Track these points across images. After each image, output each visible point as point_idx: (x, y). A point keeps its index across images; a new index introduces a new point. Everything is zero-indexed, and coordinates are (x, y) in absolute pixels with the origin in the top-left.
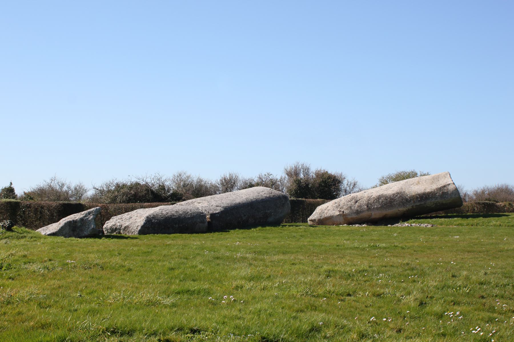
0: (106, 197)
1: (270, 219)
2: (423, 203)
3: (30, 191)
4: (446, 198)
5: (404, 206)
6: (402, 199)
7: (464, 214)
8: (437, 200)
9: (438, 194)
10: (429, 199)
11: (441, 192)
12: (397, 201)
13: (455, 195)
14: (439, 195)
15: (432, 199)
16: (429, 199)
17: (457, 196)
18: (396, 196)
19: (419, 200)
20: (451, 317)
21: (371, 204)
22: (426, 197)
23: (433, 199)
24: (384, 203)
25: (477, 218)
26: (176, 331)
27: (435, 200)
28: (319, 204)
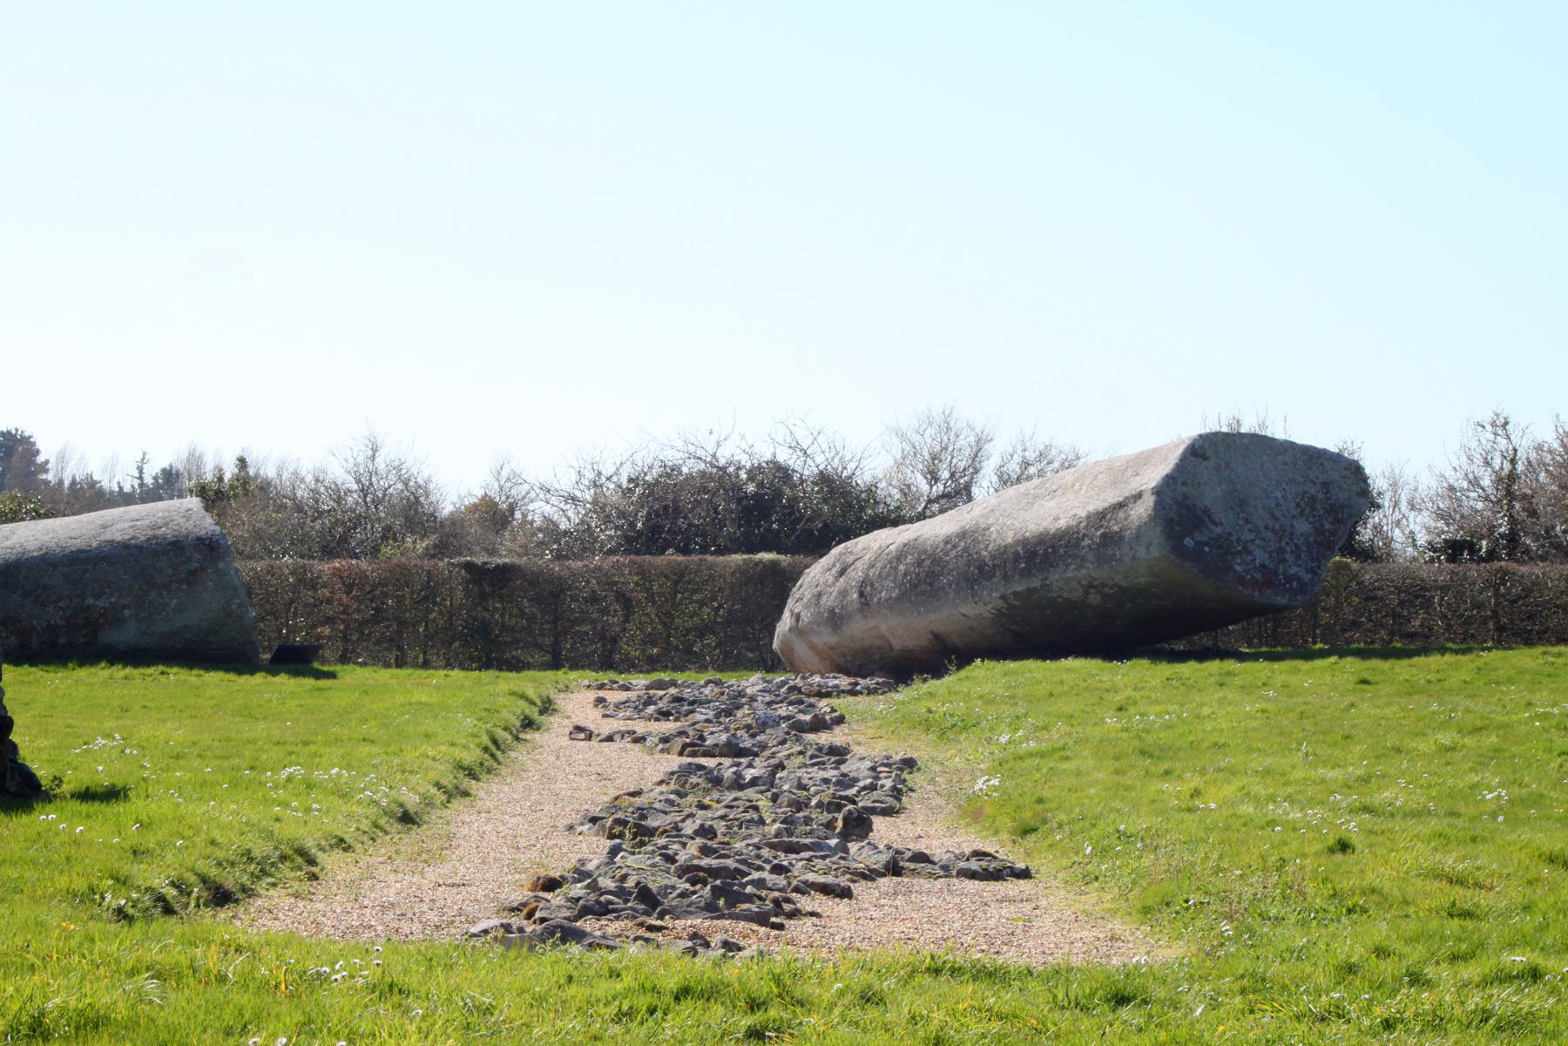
0: (51, 728)
1: (127, 634)
2: (1036, 583)
3: (270, 472)
4: (1116, 561)
5: (973, 596)
6: (968, 565)
7: (1354, 646)
8: (1084, 571)
9: (1086, 542)
10: (1058, 566)
11: (1099, 533)
12: (952, 571)
13: (1148, 549)
14: (1089, 546)
15: (1068, 565)
16: (1058, 566)
17: (1157, 555)
18: (954, 547)
19: (1023, 569)
20: (312, 668)
21: (872, 585)
22: (1046, 554)
23: (1070, 564)
24: (911, 580)
25: (1121, 660)
26: (794, 903)
27: (1078, 568)
28: (807, 567)
